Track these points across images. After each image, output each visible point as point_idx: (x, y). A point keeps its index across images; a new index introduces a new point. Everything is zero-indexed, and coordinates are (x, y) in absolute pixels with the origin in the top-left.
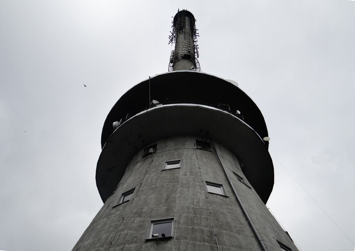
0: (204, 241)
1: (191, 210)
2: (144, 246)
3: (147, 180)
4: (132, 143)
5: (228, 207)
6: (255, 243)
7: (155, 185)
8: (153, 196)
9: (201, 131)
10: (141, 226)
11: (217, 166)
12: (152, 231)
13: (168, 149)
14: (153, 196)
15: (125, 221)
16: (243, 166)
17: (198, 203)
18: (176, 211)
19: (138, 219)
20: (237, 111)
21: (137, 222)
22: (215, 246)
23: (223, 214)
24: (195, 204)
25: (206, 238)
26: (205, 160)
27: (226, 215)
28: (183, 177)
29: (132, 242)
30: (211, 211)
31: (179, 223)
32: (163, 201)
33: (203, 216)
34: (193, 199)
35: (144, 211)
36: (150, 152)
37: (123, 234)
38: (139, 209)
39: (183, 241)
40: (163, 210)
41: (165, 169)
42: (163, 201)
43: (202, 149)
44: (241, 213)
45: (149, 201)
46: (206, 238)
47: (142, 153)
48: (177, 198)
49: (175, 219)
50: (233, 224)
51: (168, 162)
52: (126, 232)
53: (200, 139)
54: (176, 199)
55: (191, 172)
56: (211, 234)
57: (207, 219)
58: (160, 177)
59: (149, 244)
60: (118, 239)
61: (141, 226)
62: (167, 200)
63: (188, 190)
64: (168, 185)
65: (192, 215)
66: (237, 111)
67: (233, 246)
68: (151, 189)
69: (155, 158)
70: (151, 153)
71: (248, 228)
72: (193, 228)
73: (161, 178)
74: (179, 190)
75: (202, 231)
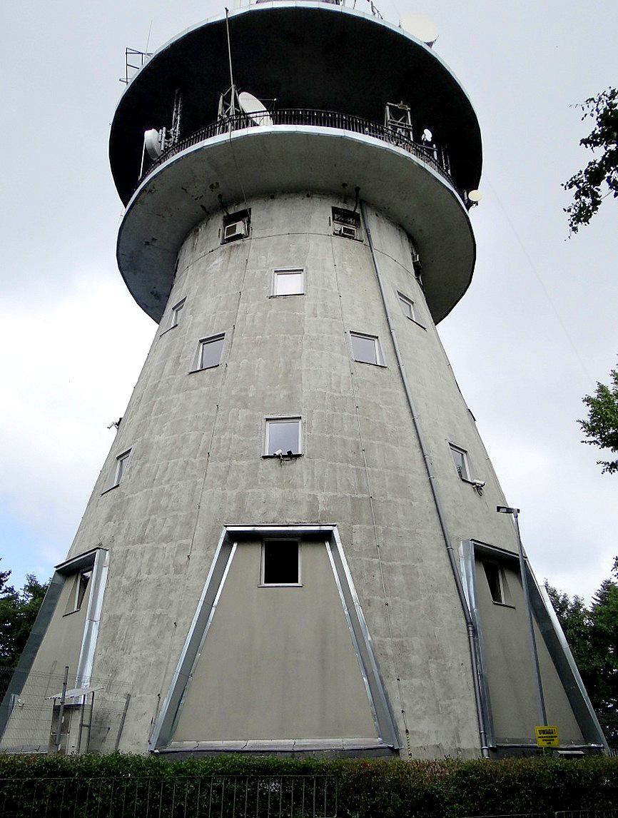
0: (348, 462)
1: (327, 402)
2: (261, 466)
3: (243, 320)
4: (196, 199)
5: (384, 390)
6: (419, 457)
7: (261, 335)
8: (260, 362)
9: (344, 185)
10: (250, 429)
11: (368, 270)
12: (271, 438)
13: (275, 231)
14: (260, 362)
15: (221, 413)
16: (418, 260)
17: (338, 386)
18: (303, 401)
19: (243, 413)
20: (426, 131)
21: (242, 419)
22: (363, 468)
23: (376, 406)
24: (334, 387)
25: (350, 455)
26: (349, 270)
27: (381, 408)
28: (311, 319)
29: (241, 457)
30: (359, 403)
31: (310, 427)
32: (280, 376)
33: (346, 414)
34: (330, 377)
35: (251, 395)
36: (238, 232)
37: (225, 439)
38: (241, 390)
39: (317, 461)
40: (282, 396)
41: (275, 294)
42: (280, 376)
43: (345, 236)
44: (403, 402)
45: (256, 373)
46: (350, 455)
47: (217, 224)
48: (303, 373)
49: (303, 419)
50: (390, 427)
51: (278, 271)
52: (227, 435)
53: (340, 206)
54: (301, 375)
55: (325, 306)
56: (358, 448)
57: (352, 418)
58: (268, 315)
59: (268, 461)
60: (218, 448)
61: (250, 429)
62: (286, 374)
63: (321, 356)
64: (285, 338)
65: (329, 412)
66: (426, 131)
67: (387, 468)
68: (256, 344)
69: (252, 254)
70: (240, 237)
71: (411, 430)
72: (331, 437)
73: (269, 318)
74: (306, 352)
75: (344, 443)
